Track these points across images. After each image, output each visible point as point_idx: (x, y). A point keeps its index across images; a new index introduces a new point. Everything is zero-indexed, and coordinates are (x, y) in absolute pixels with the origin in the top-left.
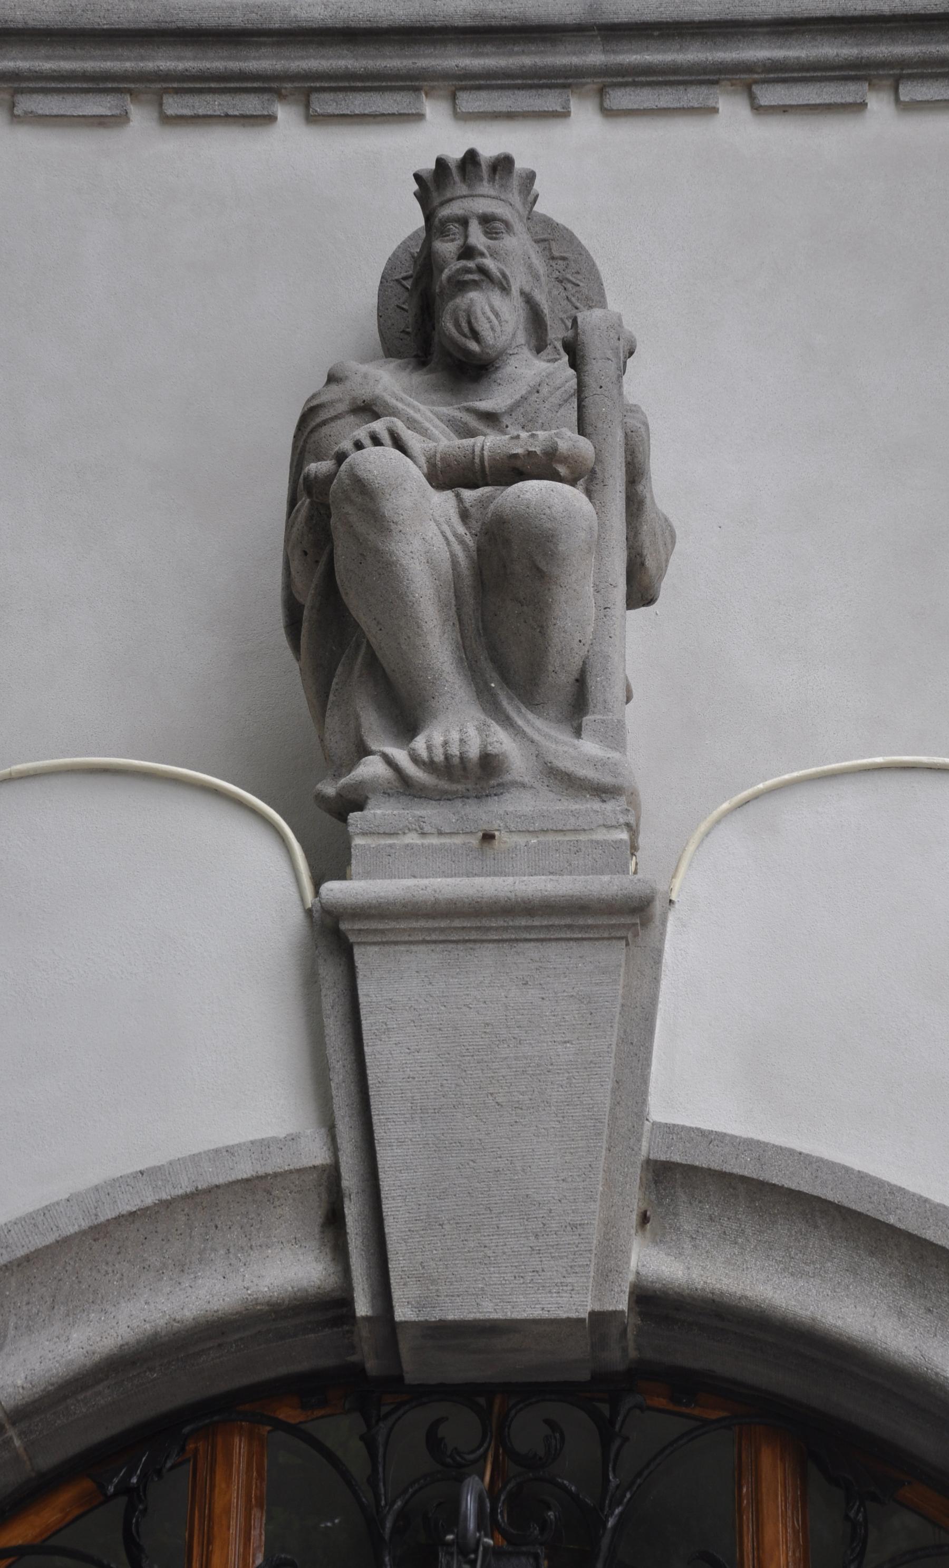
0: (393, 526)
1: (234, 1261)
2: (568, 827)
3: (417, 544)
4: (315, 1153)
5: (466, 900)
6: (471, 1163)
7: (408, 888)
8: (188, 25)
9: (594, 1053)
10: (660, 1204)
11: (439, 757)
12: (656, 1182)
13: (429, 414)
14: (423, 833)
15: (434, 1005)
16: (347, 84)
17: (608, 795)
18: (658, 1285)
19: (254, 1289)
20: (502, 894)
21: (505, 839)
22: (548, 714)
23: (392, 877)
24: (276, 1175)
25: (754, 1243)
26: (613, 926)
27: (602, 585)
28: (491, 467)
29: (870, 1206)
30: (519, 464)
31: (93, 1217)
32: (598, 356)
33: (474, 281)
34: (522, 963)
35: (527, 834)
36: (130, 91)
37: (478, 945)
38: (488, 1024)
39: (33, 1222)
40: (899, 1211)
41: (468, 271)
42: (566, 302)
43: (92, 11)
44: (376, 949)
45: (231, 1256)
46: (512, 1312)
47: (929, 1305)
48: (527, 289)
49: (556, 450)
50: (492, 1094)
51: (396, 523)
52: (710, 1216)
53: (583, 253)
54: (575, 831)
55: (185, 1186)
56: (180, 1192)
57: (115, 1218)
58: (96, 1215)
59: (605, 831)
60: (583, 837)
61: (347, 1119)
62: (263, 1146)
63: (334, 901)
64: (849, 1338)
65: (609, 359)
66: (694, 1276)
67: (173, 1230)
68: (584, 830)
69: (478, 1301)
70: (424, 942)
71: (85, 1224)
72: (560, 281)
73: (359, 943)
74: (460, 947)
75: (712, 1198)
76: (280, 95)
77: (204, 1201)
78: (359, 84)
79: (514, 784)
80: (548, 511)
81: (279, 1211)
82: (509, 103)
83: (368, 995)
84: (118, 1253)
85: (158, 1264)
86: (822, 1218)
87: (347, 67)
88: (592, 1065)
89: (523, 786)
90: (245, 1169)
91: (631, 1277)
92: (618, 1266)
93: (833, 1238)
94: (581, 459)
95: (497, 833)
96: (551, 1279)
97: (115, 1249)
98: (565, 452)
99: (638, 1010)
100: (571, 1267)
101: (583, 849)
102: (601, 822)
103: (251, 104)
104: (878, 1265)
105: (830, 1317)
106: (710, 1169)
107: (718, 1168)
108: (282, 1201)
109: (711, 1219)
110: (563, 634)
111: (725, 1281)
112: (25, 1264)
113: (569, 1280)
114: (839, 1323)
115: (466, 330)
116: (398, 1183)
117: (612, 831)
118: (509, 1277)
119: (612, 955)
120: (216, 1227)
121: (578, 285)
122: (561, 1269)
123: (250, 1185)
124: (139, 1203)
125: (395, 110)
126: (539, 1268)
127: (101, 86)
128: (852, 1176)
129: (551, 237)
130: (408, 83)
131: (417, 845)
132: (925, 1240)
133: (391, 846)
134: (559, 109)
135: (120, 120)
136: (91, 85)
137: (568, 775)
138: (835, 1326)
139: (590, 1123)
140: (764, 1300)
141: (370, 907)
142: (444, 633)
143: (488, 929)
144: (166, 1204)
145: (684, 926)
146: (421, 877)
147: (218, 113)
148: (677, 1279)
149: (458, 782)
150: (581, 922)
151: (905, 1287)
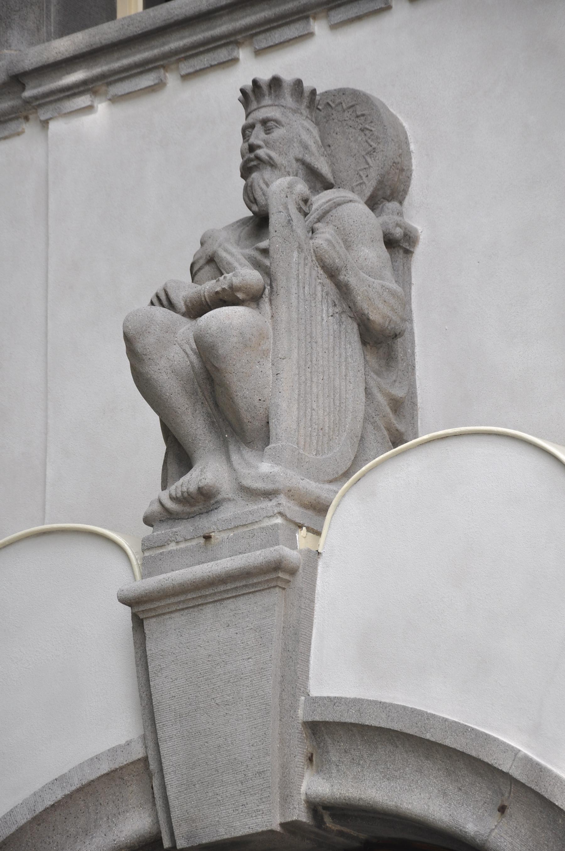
0: (144, 357)
1: (111, 824)
2: (248, 522)
3: (163, 363)
4: (138, 752)
5: (188, 582)
6: (206, 744)
7: (160, 581)
8: (180, 17)
9: (263, 663)
10: (319, 747)
11: (179, 495)
12: (314, 734)
13: (240, 257)
14: (177, 542)
15: (183, 649)
16: (269, 26)
17: (272, 496)
18: (318, 800)
19: (117, 840)
20: (205, 574)
21: (217, 537)
22: (257, 447)
23: (162, 573)
24: (121, 768)
25: (368, 762)
26: (267, 581)
27: (275, 360)
28: (211, 301)
29: (416, 730)
30: (221, 296)
31: (33, 812)
32: (274, 212)
33: (255, 166)
34: (226, 613)
35: (228, 531)
36: (163, 67)
37: (205, 606)
38: (210, 655)
39: (5, 820)
40: (432, 730)
41: (252, 160)
42: (366, 143)
43: (132, 24)
44: (154, 620)
45: (110, 821)
46: (234, 833)
47: (460, 785)
48: (300, 156)
49: (232, 285)
50: (213, 699)
51: (146, 355)
52: (345, 750)
53: (374, 108)
54: (252, 523)
55: (76, 784)
56: (74, 788)
57: (44, 810)
58: (35, 810)
59: (267, 520)
60: (256, 527)
61: (150, 727)
62: (113, 751)
63: (124, 597)
64: (415, 815)
65: (280, 212)
66: (335, 790)
67: (79, 811)
68: (257, 522)
69: (217, 828)
70: (177, 611)
71: (29, 817)
72: (362, 130)
73: (146, 618)
74: (196, 609)
75: (343, 738)
76: (238, 44)
77: (88, 790)
78: (275, 24)
79: (224, 500)
80: (209, 332)
81: (131, 789)
82: (356, 10)
83: (151, 650)
84: (54, 830)
85: (74, 833)
86: (398, 740)
87: (265, 17)
88: (263, 670)
89: (229, 500)
90: (105, 768)
91: (303, 797)
92: (291, 792)
93: (406, 752)
94: (248, 286)
95: (213, 534)
96: (251, 808)
97: (52, 828)
98: (238, 285)
99: (291, 629)
100: (261, 799)
101: (256, 534)
102: (265, 515)
103: (222, 55)
104: (431, 765)
105: (405, 804)
106: (334, 722)
107: (338, 721)
108: (131, 782)
109: (346, 752)
110: (244, 400)
111: (351, 790)
112: (4, 846)
113: (260, 807)
114: (410, 807)
115: (252, 198)
116: (171, 763)
117: (271, 519)
118: (230, 811)
119: (273, 598)
120: (101, 804)
121: (371, 131)
122: (255, 801)
123: (110, 775)
124: (55, 799)
125: (296, 35)
126: (245, 803)
127: (147, 68)
128: (408, 712)
129: (356, 103)
130: (301, 15)
131: (174, 550)
132: (446, 746)
133: (161, 554)
134: (383, 6)
135: (159, 86)
136: (139, 70)
137: (249, 489)
138: (408, 809)
139: (263, 707)
140: (371, 799)
141: (142, 597)
142: (196, 411)
143: (206, 596)
144: (69, 797)
145: (327, 567)
146: (176, 570)
147: (206, 66)
148: (326, 794)
149: (195, 506)
150: (251, 582)
151: (446, 776)
